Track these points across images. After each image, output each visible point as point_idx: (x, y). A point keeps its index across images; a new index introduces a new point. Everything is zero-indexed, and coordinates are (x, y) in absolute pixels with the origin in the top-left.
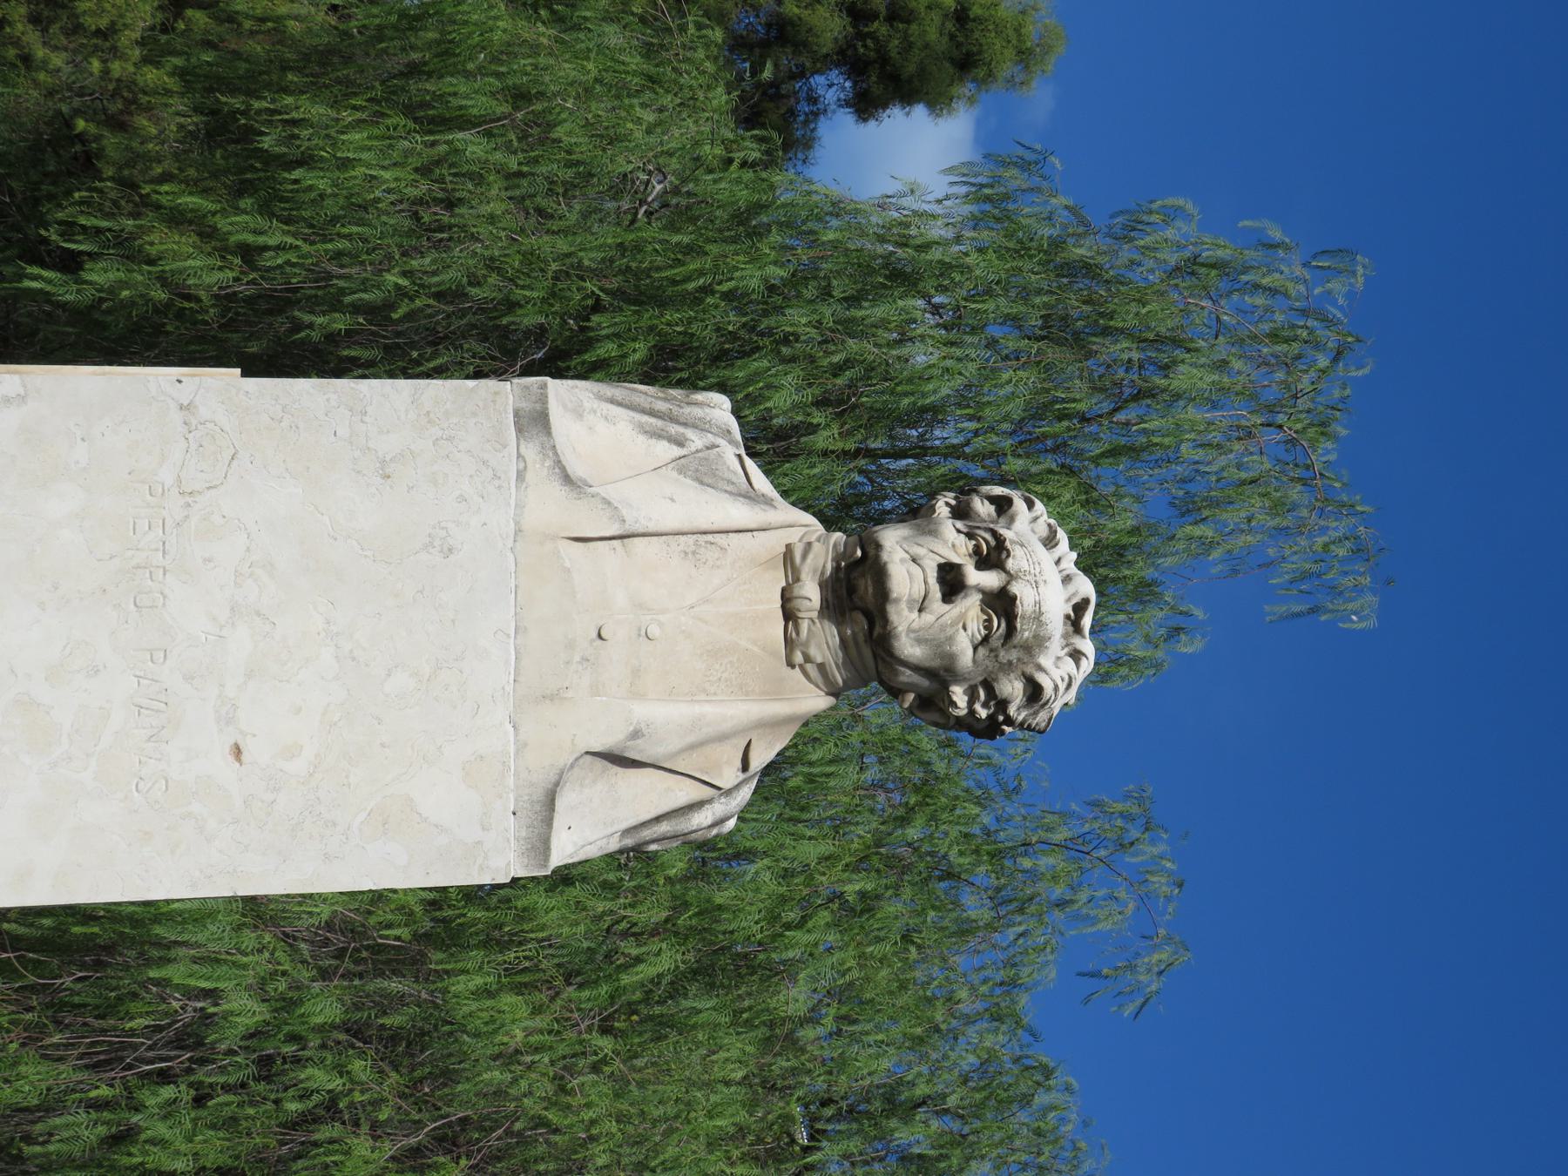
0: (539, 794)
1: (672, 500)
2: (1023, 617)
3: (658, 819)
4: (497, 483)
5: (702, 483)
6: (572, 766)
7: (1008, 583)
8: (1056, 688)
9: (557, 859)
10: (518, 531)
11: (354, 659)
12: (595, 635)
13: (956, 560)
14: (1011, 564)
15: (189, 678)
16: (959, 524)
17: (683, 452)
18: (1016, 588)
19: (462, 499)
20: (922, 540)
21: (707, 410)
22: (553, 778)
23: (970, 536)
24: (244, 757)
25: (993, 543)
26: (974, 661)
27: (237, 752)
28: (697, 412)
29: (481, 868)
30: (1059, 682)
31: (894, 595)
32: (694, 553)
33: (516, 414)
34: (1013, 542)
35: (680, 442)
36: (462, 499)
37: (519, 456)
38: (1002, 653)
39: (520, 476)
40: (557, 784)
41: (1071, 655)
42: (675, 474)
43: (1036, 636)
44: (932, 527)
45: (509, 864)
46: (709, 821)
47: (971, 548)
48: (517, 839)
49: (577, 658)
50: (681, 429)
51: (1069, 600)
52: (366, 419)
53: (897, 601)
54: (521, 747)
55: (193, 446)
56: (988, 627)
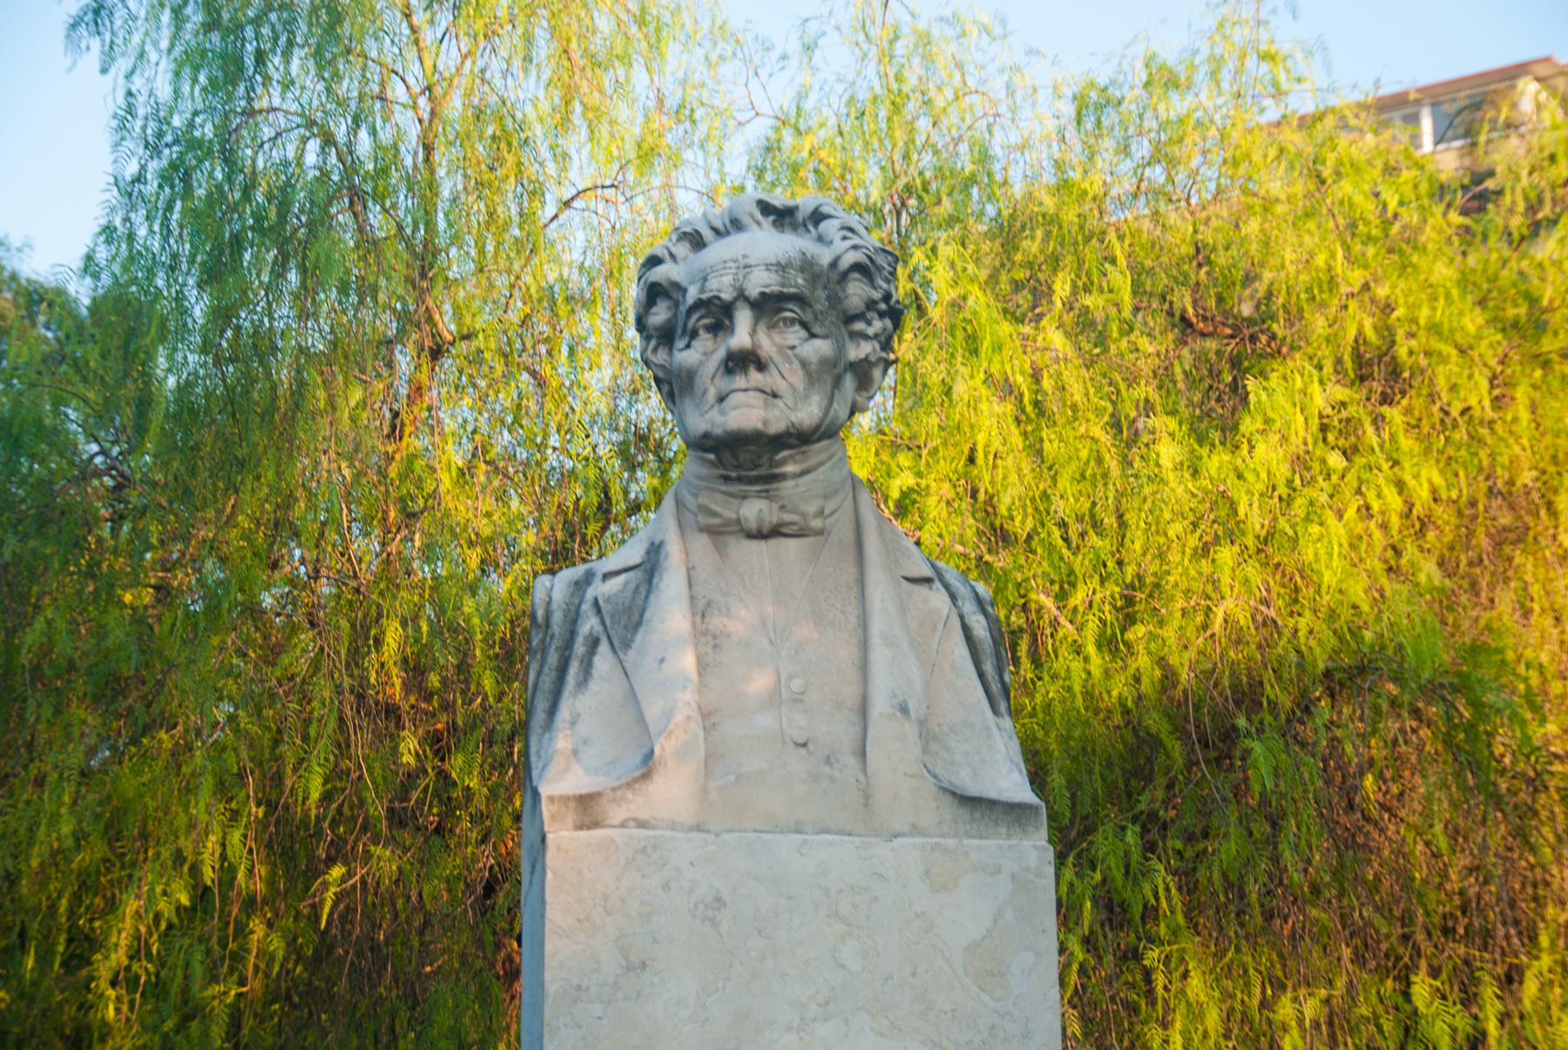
0: (964, 813)
1: (662, 660)
2: (783, 285)
3: (981, 675)
4: (650, 850)
5: (639, 624)
6: (935, 777)
7: (747, 299)
8: (855, 247)
9: (1026, 795)
10: (698, 828)
11: (827, 1003)
12: (803, 751)
13: (721, 354)
14: (727, 296)
16: (680, 344)
17: (604, 640)
18: (753, 291)
20: (698, 389)
21: (554, 606)
22: (948, 798)
23: (694, 335)
25: (703, 311)
26: (825, 337)
28: (557, 617)
29: (1039, 875)
30: (848, 243)
31: (760, 426)
32: (715, 637)
33: (580, 827)
34: (702, 290)
35: (594, 643)
36: (666, 887)
37: (623, 825)
38: (818, 307)
39: (642, 824)
40: (954, 794)
41: (816, 224)
42: (631, 653)
43: (802, 270)
44: (684, 375)
45: (1035, 847)
46: (981, 618)
47: (709, 336)
48: (1009, 837)
49: (827, 769)
50: (580, 640)
51: (758, 223)
52: (584, 985)
54: (916, 830)
56: (792, 321)
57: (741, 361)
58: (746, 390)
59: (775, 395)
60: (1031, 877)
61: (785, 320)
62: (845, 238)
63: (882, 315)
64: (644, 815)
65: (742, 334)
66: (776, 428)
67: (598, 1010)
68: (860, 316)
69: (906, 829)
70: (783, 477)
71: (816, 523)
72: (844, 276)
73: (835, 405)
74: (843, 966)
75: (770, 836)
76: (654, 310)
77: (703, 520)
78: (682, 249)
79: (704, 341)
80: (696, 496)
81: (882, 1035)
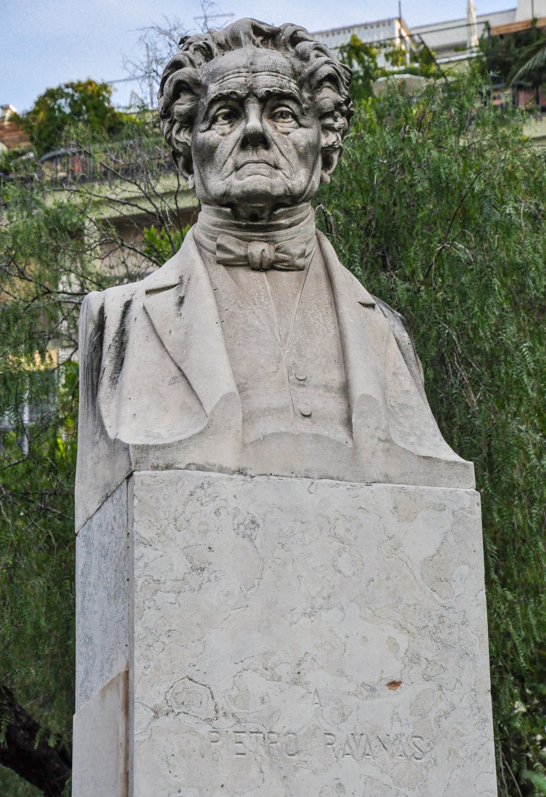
4: (206, 486)
7: (255, 95)
10: (241, 472)
12: (307, 420)
14: (241, 92)
15: (344, 718)
19: (217, 512)
23: (214, 120)
24: (397, 678)
25: (222, 103)
27: (394, 684)
31: (269, 189)
34: (221, 88)
36: (217, 512)
39: (201, 468)
52: (163, 580)
53: (272, 186)
54: (388, 480)
55: (183, 709)
57: (255, 141)
58: (257, 162)
59: (276, 167)
60: (465, 513)
61: (282, 112)
62: (317, 56)
63: (343, 114)
64: (200, 461)
65: (254, 120)
66: (279, 190)
67: (172, 597)
68: (330, 114)
69: (381, 478)
70: (280, 227)
71: (300, 262)
72: (320, 83)
73: (314, 177)
74: (340, 571)
75: (289, 480)
76: (179, 101)
77: (220, 255)
78: (199, 58)
79: (221, 126)
80: (214, 239)
81: (366, 619)
